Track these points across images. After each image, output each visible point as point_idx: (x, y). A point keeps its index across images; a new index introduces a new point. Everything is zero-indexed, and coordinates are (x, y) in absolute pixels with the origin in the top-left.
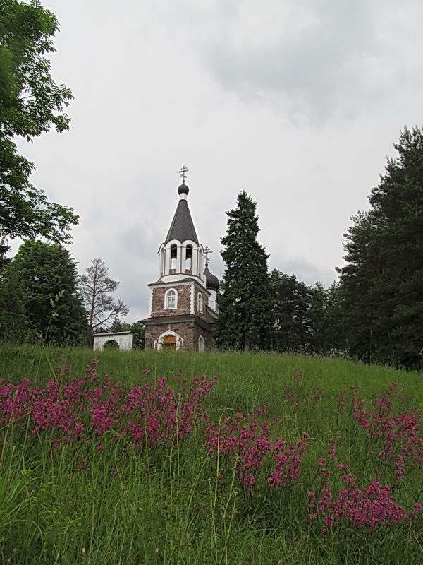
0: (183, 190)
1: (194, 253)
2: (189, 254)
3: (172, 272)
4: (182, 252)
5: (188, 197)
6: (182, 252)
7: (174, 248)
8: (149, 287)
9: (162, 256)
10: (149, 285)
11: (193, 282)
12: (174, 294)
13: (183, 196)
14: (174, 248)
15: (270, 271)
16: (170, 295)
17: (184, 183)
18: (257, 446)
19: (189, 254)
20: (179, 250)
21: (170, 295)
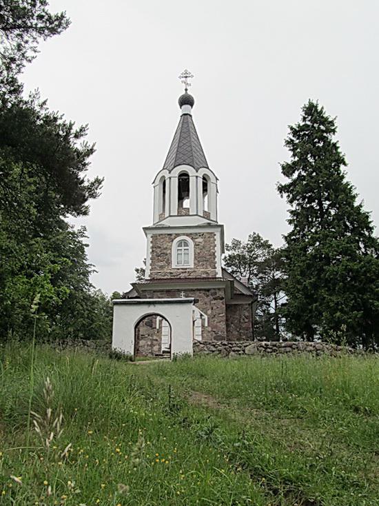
0: (186, 101)
5: (193, 111)
6: (195, 185)
12: (186, 245)
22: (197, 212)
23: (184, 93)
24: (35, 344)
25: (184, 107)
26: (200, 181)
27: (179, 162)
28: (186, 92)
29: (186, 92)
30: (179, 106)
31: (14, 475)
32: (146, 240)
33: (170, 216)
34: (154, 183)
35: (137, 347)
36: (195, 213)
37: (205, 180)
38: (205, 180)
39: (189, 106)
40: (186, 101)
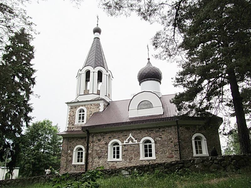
0: (97, 31)
1: (104, 77)
2: (100, 79)
3: (86, 93)
4: (94, 76)
5: (101, 36)
6: (94, 76)
7: (88, 73)
8: (66, 104)
9: (79, 80)
10: (67, 103)
11: (102, 101)
12: (84, 111)
13: (97, 34)
14: (88, 73)
15: (235, 117)
16: (80, 112)
17: (149, 63)
18: (225, 113)
19: (100, 79)
20: (91, 74)
21: (80, 112)
22: (93, 92)
23: (96, 26)
24: (74, 125)
25: (96, 33)
26: (96, 74)
27: (86, 65)
28: (97, 26)
29: (97, 26)
30: (93, 33)
31: (199, 159)
32: (146, 65)
33: (80, 95)
34: (77, 77)
35: (144, 129)
36: (92, 93)
37: (100, 74)
38: (100, 74)
39: (99, 34)
40: (97, 31)
